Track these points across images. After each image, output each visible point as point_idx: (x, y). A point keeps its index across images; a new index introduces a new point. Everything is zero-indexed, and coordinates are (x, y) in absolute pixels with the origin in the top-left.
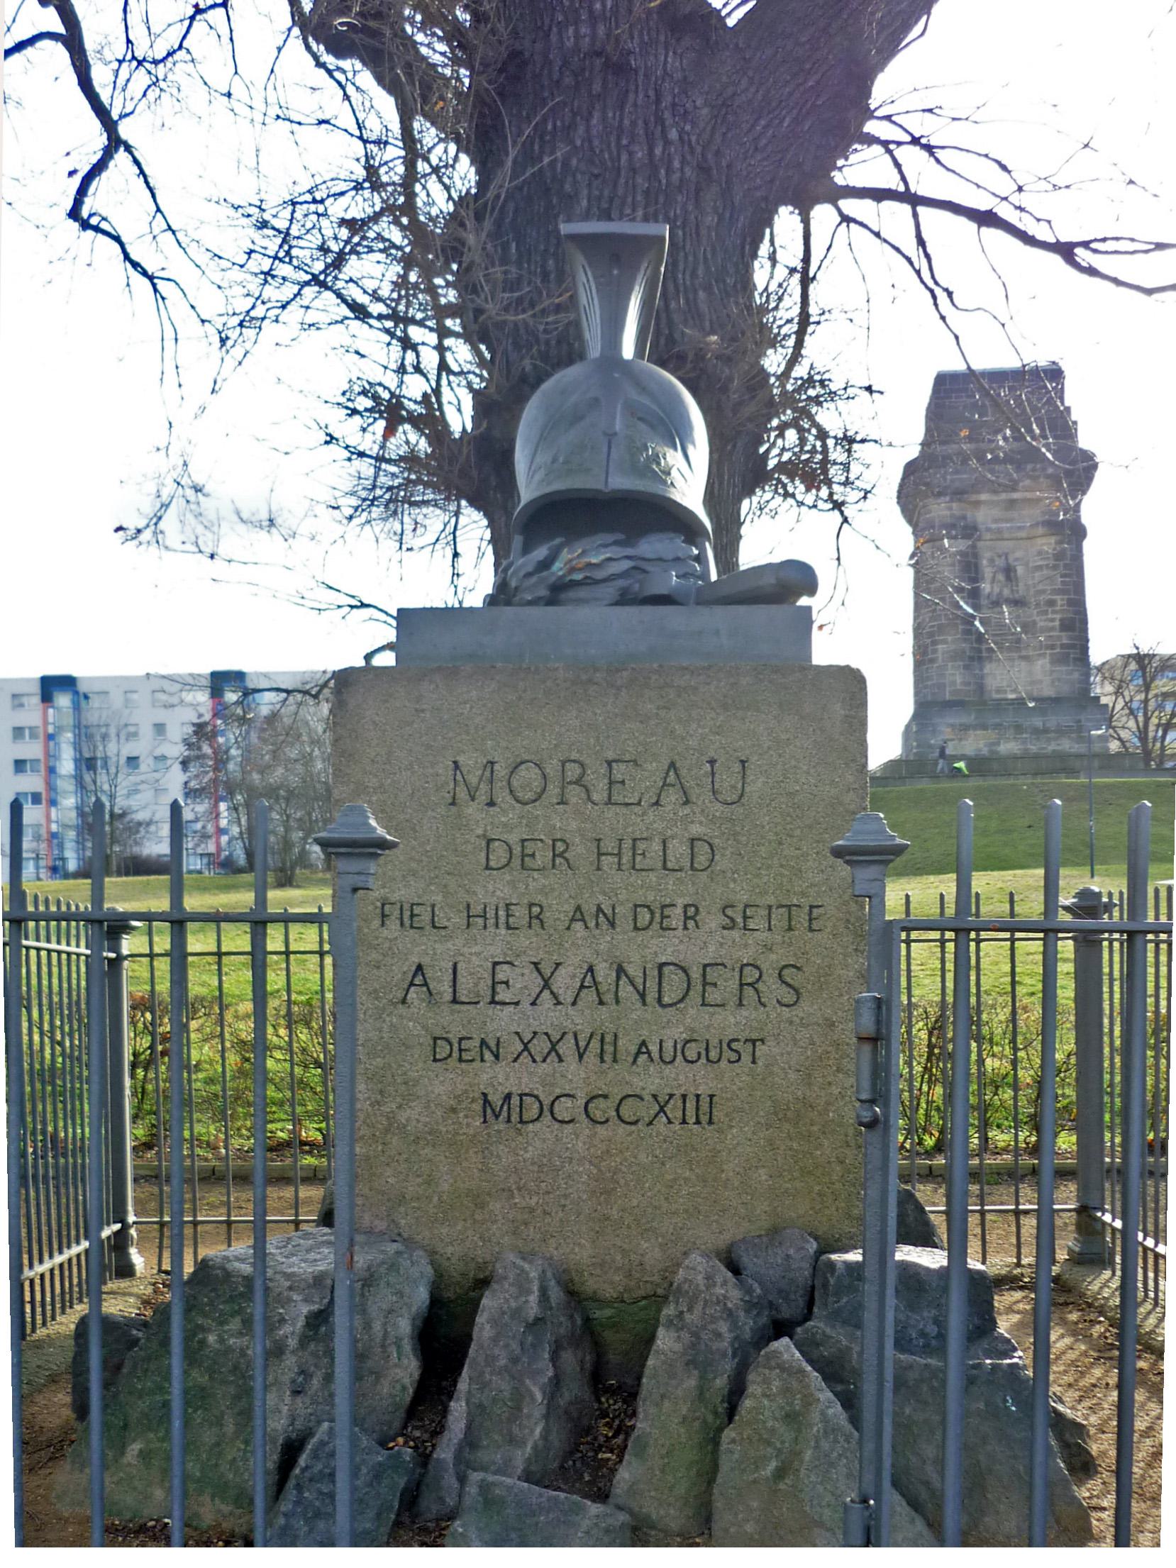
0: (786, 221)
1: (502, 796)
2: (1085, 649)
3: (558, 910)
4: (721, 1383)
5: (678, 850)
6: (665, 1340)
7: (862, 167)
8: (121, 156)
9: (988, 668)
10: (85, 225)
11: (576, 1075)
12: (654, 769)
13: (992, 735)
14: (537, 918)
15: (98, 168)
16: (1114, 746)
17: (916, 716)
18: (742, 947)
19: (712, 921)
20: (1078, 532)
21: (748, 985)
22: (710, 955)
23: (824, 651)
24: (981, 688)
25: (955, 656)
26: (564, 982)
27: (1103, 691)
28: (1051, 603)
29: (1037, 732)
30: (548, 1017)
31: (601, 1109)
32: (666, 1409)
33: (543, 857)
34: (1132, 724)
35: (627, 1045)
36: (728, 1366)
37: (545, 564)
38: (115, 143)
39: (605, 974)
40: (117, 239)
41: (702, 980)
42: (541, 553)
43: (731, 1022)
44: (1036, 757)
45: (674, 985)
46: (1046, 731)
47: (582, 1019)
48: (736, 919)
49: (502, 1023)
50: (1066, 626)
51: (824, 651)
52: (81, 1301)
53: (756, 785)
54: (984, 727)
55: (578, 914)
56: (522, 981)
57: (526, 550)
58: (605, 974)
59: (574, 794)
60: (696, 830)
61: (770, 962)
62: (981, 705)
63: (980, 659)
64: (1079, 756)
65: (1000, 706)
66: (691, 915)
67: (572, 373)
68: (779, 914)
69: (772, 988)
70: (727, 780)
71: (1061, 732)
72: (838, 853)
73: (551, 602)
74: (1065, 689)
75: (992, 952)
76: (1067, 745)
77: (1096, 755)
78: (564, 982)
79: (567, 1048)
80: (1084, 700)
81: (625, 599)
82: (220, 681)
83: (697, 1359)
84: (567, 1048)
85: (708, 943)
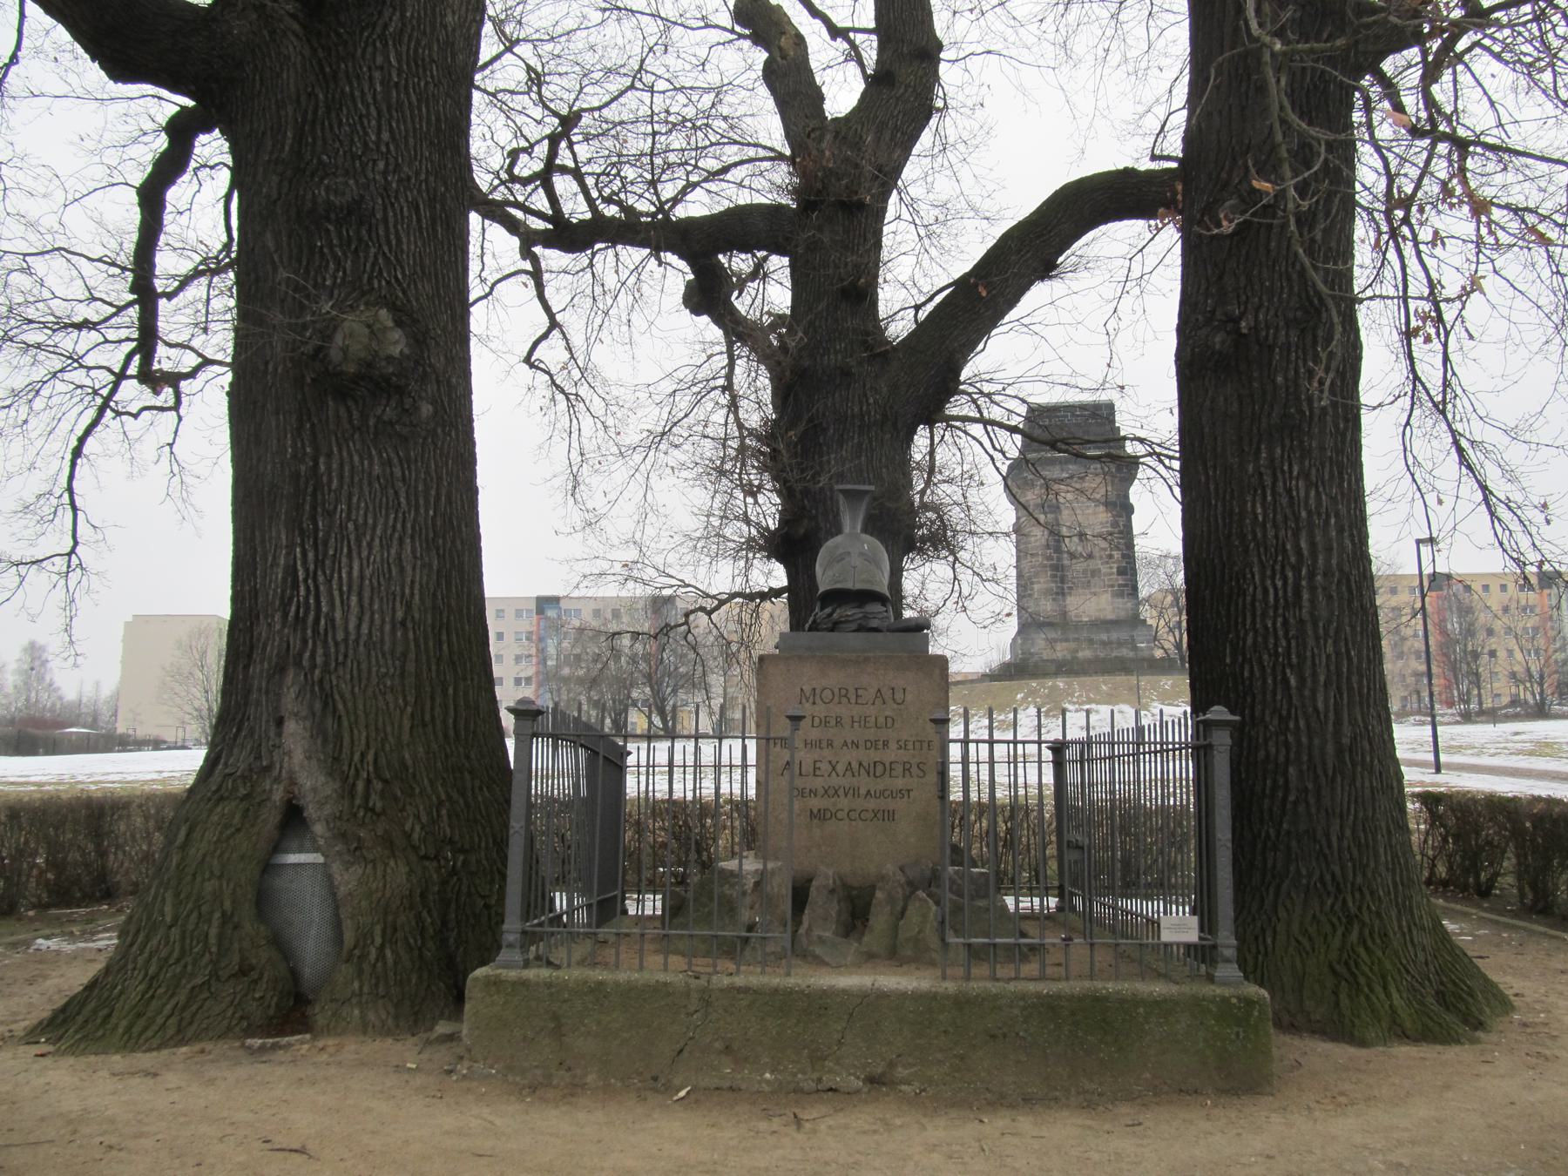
0: (921, 440)
1: (818, 700)
2: (1135, 589)
3: (838, 743)
4: (899, 908)
5: (881, 720)
6: (879, 895)
7: (958, 406)
8: (556, 333)
9: (1069, 600)
10: (532, 366)
11: (844, 803)
12: (873, 691)
13: (1073, 645)
14: (830, 744)
15: (545, 336)
16: (1159, 653)
17: (1019, 633)
18: (903, 756)
19: (893, 745)
20: (1129, 509)
21: (907, 770)
22: (893, 758)
23: (933, 650)
24: (1064, 614)
25: (1048, 592)
26: (840, 768)
27: (1147, 613)
28: (1111, 556)
29: (1104, 644)
30: (835, 781)
31: (854, 815)
32: (879, 920)
33: (833, 722)
34: (1171, 638)
35: (863, 791)
36: (901, 903)
37: (830, 615)
38: (554, 324)
39: (855, 765)
40: (548, 373)
41: (889, 769)
42: (828, 610)
43: (900, 783)
44: (1104, 660)
45: (880, 769)
46: (1110, 643)
47: (846, 782)
48: (902, 746)
49: (818, 783)
50: (1121, 572)
51: (933, 650)
52: (1324, 409)
53: (909, 697)
54: (1067, 640)
55: (845, 744)
56: (825, 767)
57: (822, 609)
58: (855, 765)
59: (844, 700)
60: (887, 713)
61: (914, 761)
62: (1062, 624)
63: (1063, 594)
64: (1133, 660)
65: (1078, 626)
66: (886, 744)
67: (838, 539)
68: (918, 745)
69: (914, 770)
70: (899, 696)
71: (1120, 644)
72: (933, 721)
73: (832, 630)
74: (1122, 614)
75: (972, 746)
76: (1125, 652)
77: (1144, 659)
78: (840, 768)
79: (841, 792)
80: (1135, 621)
81: (859, 629)
82: (545, 603)
83: (891, 899)
84: (841, 792)
85: (891, 755)
